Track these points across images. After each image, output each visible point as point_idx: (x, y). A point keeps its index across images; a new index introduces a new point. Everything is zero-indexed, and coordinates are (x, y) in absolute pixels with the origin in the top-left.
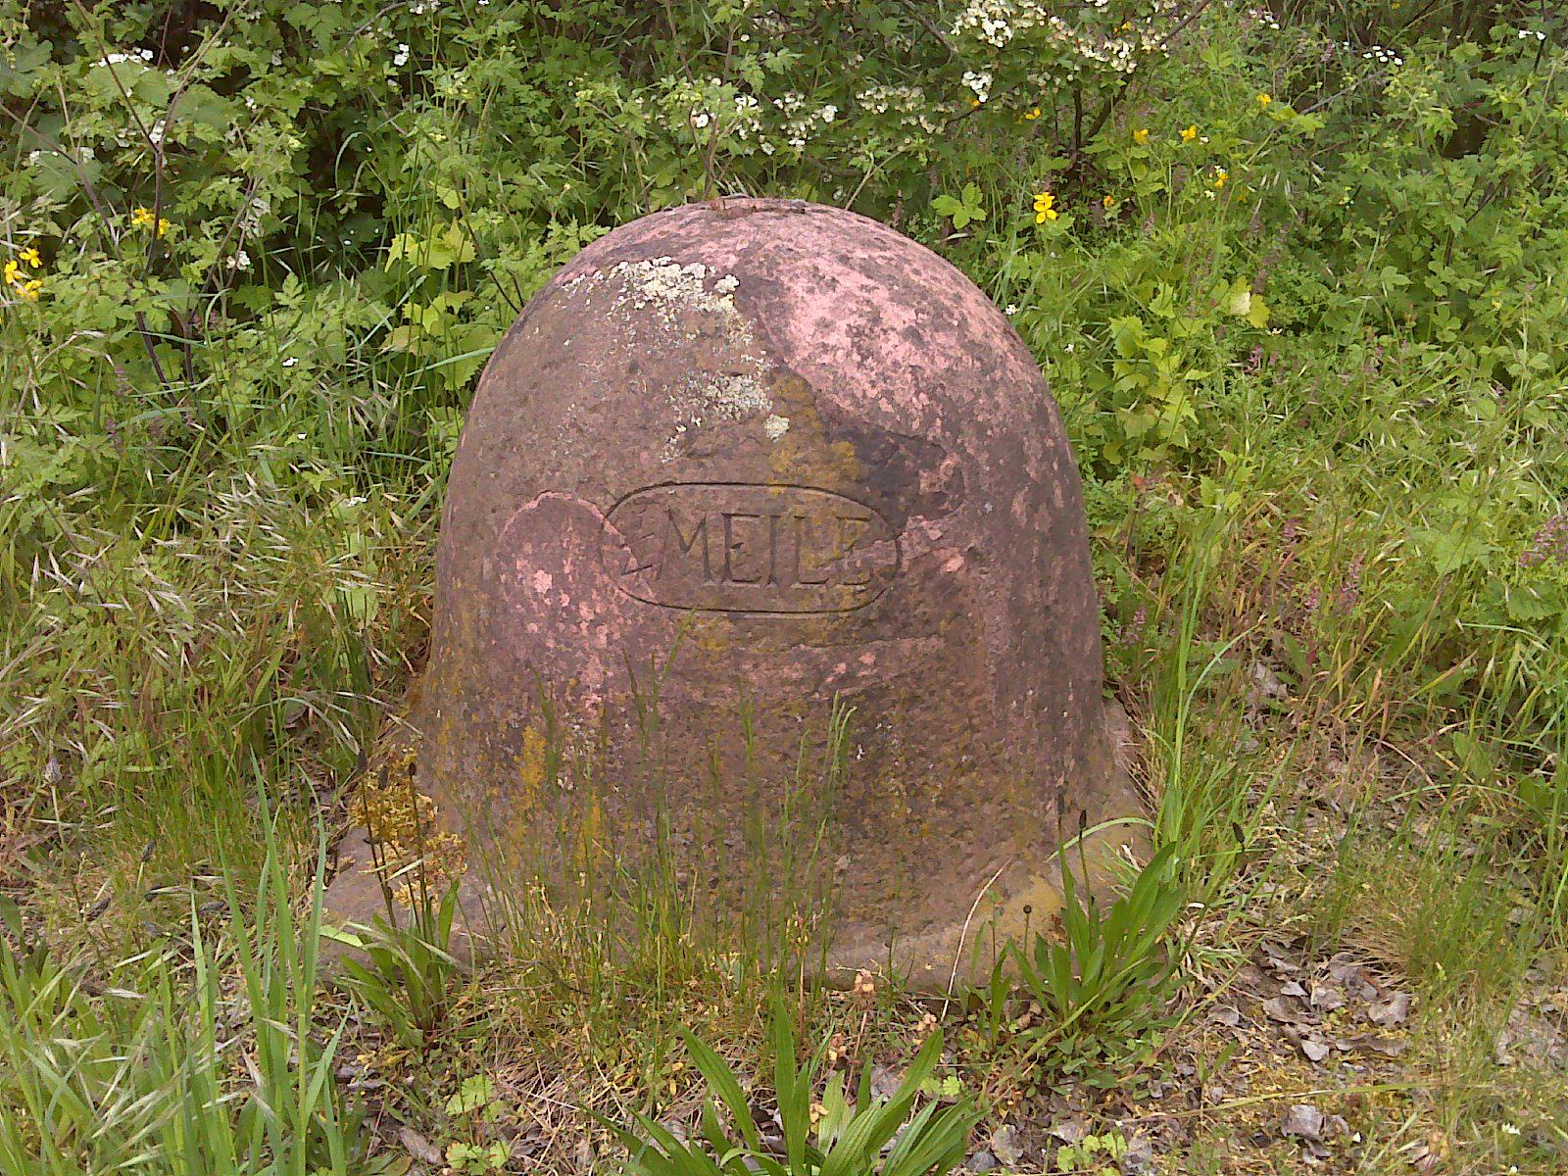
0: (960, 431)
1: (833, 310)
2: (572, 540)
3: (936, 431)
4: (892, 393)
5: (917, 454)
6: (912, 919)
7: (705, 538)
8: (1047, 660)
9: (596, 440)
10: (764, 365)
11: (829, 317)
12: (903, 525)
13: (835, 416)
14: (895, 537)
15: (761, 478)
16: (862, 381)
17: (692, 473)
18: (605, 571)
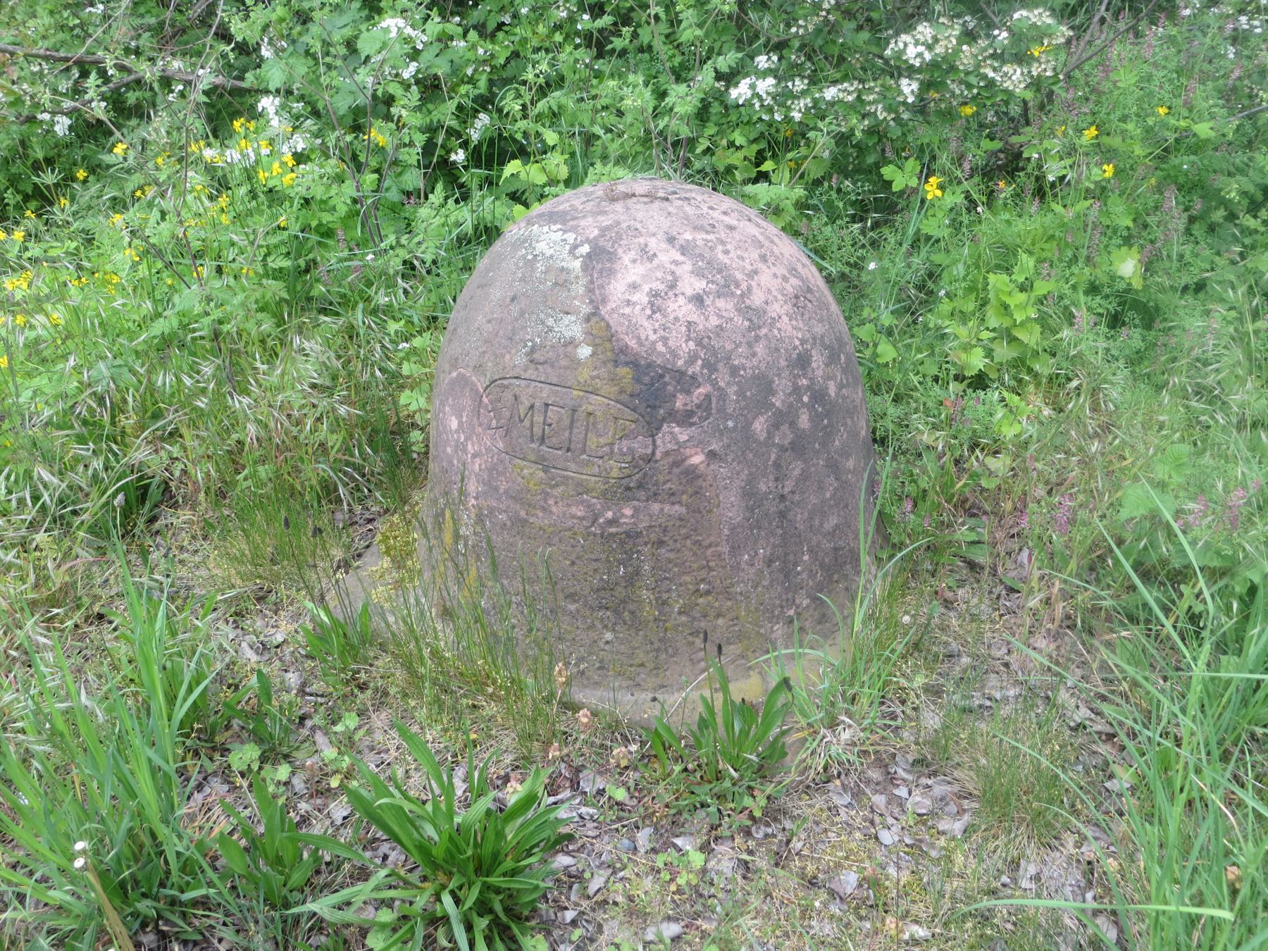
0: (716, 370)
1: (643, 276)
2: (467, 402)
3: (697, 368)
4: (667, 339)
5: (678, 383)
6: (652, 682)
7: (532, 416)
8: (780, 531)
9: (486, 342)
10: (586, 309)
11: (639, 281)
12: (659, 429)
13: (624, 350)
14: (653, 436)
15: (569, 384)
16: (648, 330)
17: (531, 373)
18: (480, 425)
